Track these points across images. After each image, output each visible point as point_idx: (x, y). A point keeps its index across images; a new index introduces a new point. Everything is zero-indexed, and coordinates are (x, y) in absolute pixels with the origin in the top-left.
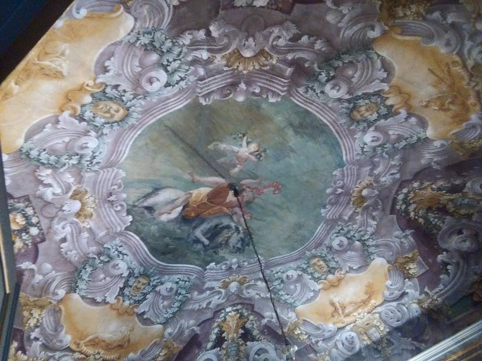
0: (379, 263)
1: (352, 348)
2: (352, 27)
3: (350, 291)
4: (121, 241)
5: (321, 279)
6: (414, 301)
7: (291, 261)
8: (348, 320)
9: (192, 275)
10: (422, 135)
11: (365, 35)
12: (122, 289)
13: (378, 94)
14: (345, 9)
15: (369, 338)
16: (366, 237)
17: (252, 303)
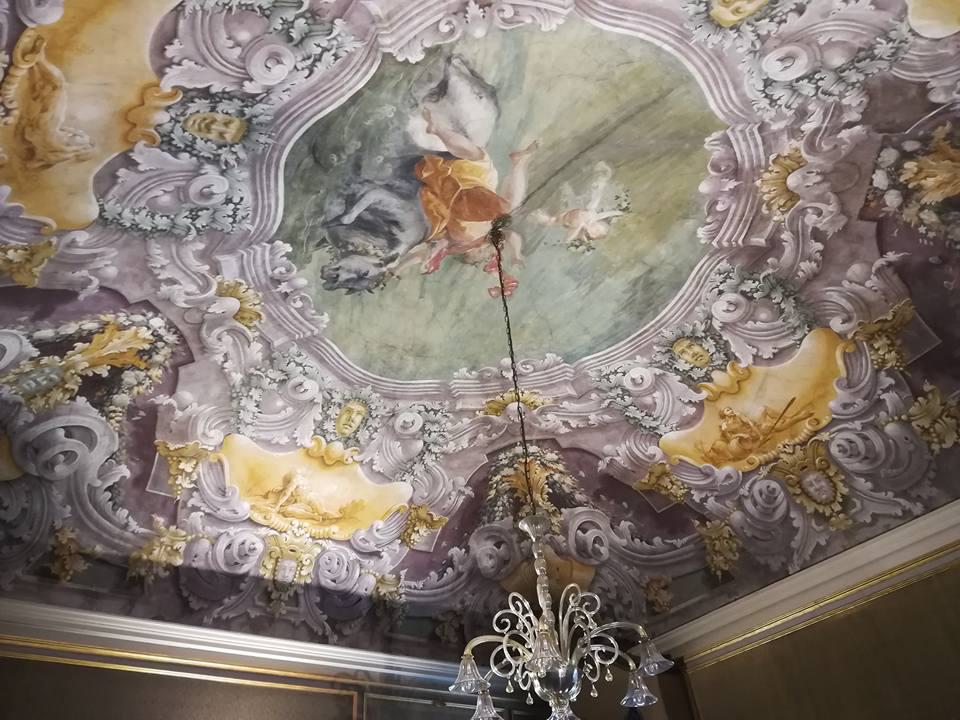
0: (402, 492)
1: (236, 563)
2: (844, 297)
3: (325, 489)
4: (350, 55)
5: (324, 436)
6: (377, 574)
7: (336, 373)
8: (277, 521)
9: (253, 223)
10: (662, 430)
11: (833, 315)
12: (205, 93)
13: (730, 357)
14: (873, 282)
15: (275, 570)
16: (435, 449)
17: (197, 357)
